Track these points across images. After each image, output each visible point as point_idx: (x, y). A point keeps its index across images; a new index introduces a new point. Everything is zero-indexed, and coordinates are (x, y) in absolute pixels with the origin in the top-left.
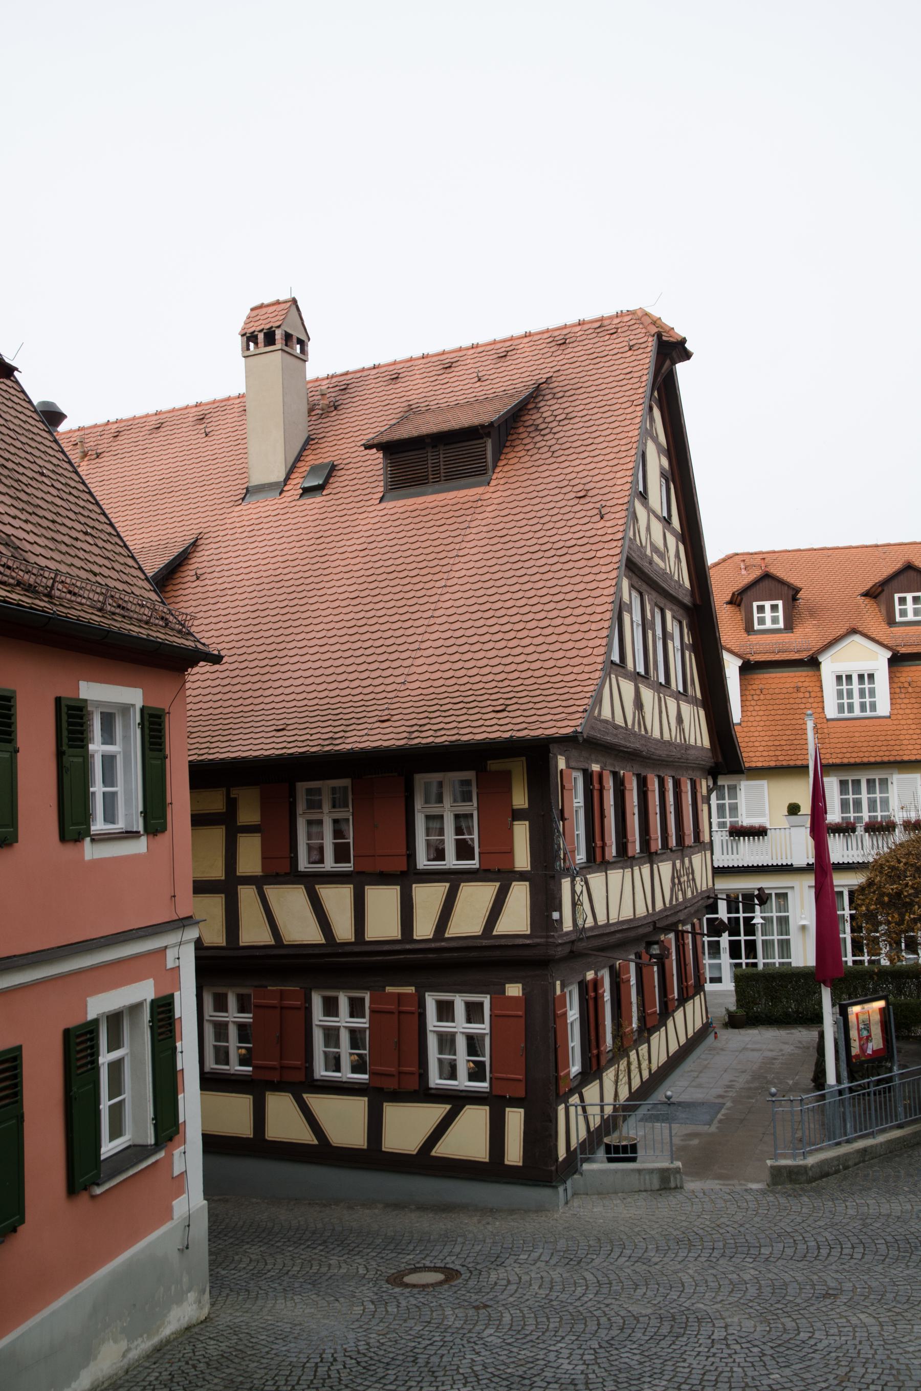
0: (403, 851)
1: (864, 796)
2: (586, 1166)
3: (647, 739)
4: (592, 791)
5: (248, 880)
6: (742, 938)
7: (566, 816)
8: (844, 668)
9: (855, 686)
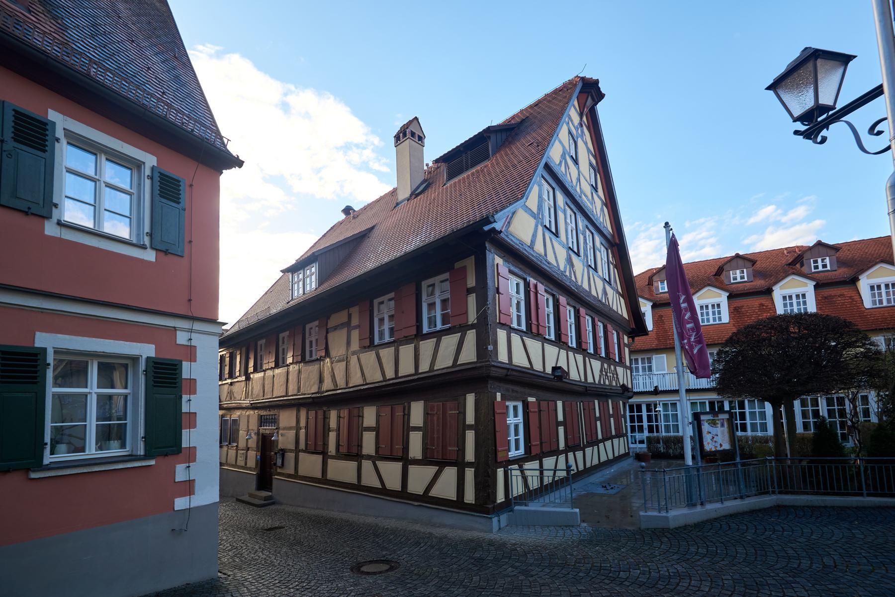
0: (414, 322)
1: (640, 365)
3: (611, 309)
4: (529, 292)
5: (369, 457)
7: (500, 291)
9: (794, 300)
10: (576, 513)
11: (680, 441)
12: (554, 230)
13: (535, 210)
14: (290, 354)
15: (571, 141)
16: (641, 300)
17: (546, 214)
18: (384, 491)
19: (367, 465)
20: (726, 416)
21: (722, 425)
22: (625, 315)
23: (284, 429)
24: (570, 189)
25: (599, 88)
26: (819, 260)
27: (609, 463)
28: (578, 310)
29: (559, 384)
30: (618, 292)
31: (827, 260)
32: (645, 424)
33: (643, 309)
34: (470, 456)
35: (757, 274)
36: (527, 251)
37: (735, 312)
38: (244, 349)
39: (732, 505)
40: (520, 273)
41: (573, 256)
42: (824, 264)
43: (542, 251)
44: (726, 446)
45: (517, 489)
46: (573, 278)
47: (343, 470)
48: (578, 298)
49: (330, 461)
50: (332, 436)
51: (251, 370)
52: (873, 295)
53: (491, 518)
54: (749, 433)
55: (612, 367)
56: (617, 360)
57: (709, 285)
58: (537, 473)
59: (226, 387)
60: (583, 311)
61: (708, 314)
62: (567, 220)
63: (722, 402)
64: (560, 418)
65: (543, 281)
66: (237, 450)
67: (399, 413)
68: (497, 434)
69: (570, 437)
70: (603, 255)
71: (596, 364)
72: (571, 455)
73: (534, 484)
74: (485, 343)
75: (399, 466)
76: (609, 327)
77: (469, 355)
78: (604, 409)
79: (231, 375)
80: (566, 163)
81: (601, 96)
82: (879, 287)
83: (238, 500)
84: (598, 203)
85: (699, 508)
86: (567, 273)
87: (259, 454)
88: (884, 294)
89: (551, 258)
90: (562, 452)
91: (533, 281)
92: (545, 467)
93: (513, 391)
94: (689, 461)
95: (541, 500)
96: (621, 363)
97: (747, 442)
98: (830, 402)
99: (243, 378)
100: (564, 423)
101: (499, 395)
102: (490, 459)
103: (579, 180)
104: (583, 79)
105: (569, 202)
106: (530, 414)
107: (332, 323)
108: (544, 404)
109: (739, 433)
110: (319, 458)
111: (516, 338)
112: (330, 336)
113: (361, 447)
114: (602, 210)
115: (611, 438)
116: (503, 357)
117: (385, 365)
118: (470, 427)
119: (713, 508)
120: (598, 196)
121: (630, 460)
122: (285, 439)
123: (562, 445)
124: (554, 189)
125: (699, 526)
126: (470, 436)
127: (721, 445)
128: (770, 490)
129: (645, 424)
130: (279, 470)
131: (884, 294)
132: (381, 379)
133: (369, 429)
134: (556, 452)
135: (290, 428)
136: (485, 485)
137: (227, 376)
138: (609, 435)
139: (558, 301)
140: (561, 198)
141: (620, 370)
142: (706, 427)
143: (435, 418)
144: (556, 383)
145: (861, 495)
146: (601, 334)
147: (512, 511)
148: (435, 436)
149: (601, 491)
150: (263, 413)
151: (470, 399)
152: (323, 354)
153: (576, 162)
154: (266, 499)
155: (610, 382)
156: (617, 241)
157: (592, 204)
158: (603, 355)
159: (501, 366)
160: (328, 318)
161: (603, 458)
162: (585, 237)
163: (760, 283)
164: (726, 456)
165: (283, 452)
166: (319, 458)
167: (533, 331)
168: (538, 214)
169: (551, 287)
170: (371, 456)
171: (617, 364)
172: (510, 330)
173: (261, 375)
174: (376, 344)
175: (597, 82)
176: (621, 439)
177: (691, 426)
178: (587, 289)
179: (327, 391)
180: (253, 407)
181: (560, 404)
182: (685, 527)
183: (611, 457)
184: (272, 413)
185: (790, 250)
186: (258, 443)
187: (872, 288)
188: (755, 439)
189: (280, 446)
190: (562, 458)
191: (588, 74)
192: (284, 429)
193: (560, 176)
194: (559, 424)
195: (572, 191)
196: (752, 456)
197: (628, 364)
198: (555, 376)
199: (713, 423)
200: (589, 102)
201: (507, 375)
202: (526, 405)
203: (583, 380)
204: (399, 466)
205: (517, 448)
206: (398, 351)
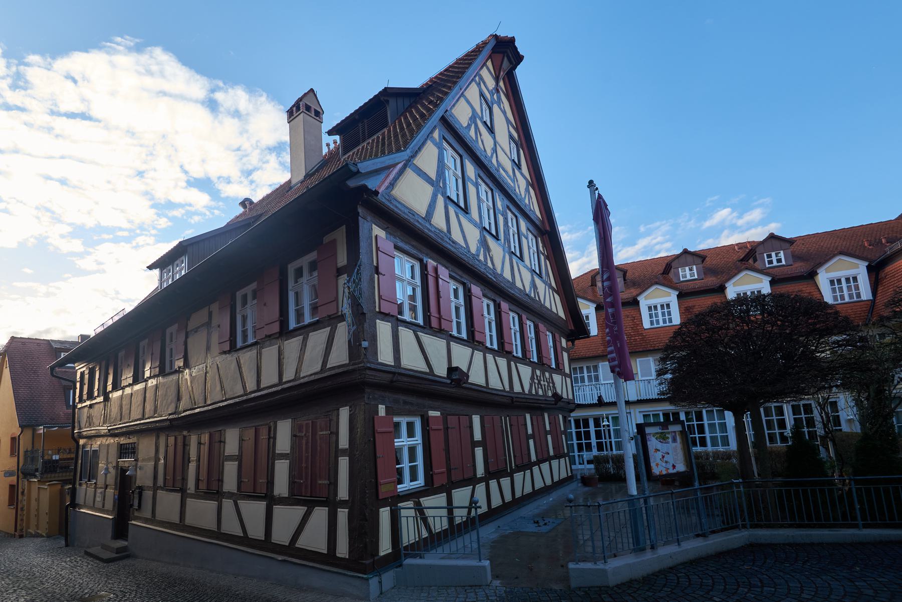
1: (586, 375)
2: (408, 561)
3: (543, 306)
4: (427, 275)
5: (230, 495)
6: (584, 441)
8: (652, 302)
10: (484, 567)
11: (619, 461)
12: (462, 204)
13: (433, 175)
14: (148, 367)
15: (484, 106)
16: (579, 300)
17: (485, 215)
18: (245, 540)
19: (228, 504)
20: (678, 428)
21: (674, 440)
22: (562, 314)
23: (144, 460)
24: (482, 158)
25: (516, 48)
26: (773, 254)
27: (546, 490)
28: (499, 305)
29: (453, 390)
30: (551, 287)
31: (782, 255)
32: (594, 441)
33: (584, 312)
34: (343, 493)
35: (708, 271)
36: (421, 225)
37: (684, 311)
38: (103, 364)
39: (693, 547)
40: (414, 251)
41: (490, 240)
42: (779, 258)
43: (443, 226)
44: (681, 467)
45: (410, 534)
46: (490, 264)
47: (202, 512)
48: (498, 290)
49: (190, 502)
50: (192, 467)
51: (109, 388)
52: (834, 290)
53: (367, 579)
54: (710, 448)
55: (547, 374)
56: (554, 366)
57: (657, 283)
58: (444, 512)
59: (86, 409)
60: (505, 306)
61: (657, 316)
62: (480, 196)
63: (678, 414)
64: (478, 436)
65: (445, 262)
66: (96, 488)
67: (264, 436)
68: (378, 460)
69: (491, 460)
70: (531, 245)
71: (526, 371)
72: (493, 483)
73: (460, 515)
74: (361, 343)
75: (262, 505)
76: (542, 327)
77: (340, 356)
78: (538, 425)
79: (91, 396)
80: (477, 129)
81: (519, 59)
82: (839, 281)
83: (87, 553)
84: (522, 183)
85: (648, 555)
86: (481, 258)
87: (117, 492)
88: (845, 289)
89: (456, 235)
90: (480, 480)
91: (431, 263)
92: (455, 504)
93: (405, 403)
94: (633, 490)
95: (440, 550)
96: (559, 369)
97: (708, 459)
98: (796, 410)
99: (101, 399)
100: (483, 443)
101: (382, 410)
102: (369, 496)
103: (495, 150)
104: (496, 37)
105: (482, 174)
106: (431, 433)
107: (192, 325)
108: (452, 420)
109: (699, 449)
110: (177, 496)
111: (406, 334)
112: (189, 340)
113: (222, 481)
114: (527, 190)
115: (549, 459)
116: (385, 356)
117: (245, 374)
118: (344, 452)
119: (668, 553)
120: (522, 174)
121: (575, 485)
122: (143, 477)
123: (480, 471)
124: (461, 156)
125: (649, 580)
126: (344, 464)
127: (674, 467)
128: (740, 523)
129: (594, 441)
130: (136, 514)
131: (845, 289)
132: (242, 392)
133: (230, 458)
134: (472, 481)
135: (149, 459)
136: (364, 532)
137: (85, 397)
138: (546, 456)
139: (470, 290)
140: (471, 170)
141: (557, 378)
142: (653, 443)
143: (304, 442)
144: (454, 391)
145: (856, 526)
146: (531, 335)
147: (401, 565)
148: (304, 465)
149: (531, 528)
150: (123, 440)
151: (344, 414)
152: (182, 364)
153: (491, 130)
154: (118, 551)
155: (545, 392)
156: (548, 228)
157: (514, 182)
158: (535, 360)
159: (383, 369)
160: (188, 319)
161: (539, 484)
162: (506, 219)
163: (712, 281)
164: (683, 479)
165: (141, 489)
166: (177, 496)
167: (433, 324)
168: (438, 181)
169: (460, 273)
170: (233, 494)
171: (552, 371)
172: (397, 322)
173: (119, 393)
174: (238, 347)
175: (512, 40)
176: (562, 460)
177: (633, 442)
178: (510, 279)
179: (184, 411)
180: (112, 434)
181: (476, 419)
182: (630, 583)
183: (549, 482)
184: (131, 441)
185: (741, 246)
186: (116, 479)
187: (832, 282)
188: (716, 455)
189: (139, 483)
190: (481, 488)
191: (502, 33)
192: (144, 460)
193: (468, 141)
194: (475, 444)
195: (486, 162)
196: (714, 477)
197: (567, 371)
198: (452, 380)
199: (663, 438)
200: (506, 65)
201: (392, 381)
202: (426, 421)
203: (507, 388)
204: (262, 505)
205: (414, 478)
206: (261, 354)
